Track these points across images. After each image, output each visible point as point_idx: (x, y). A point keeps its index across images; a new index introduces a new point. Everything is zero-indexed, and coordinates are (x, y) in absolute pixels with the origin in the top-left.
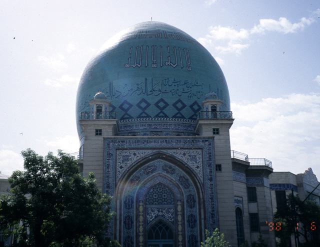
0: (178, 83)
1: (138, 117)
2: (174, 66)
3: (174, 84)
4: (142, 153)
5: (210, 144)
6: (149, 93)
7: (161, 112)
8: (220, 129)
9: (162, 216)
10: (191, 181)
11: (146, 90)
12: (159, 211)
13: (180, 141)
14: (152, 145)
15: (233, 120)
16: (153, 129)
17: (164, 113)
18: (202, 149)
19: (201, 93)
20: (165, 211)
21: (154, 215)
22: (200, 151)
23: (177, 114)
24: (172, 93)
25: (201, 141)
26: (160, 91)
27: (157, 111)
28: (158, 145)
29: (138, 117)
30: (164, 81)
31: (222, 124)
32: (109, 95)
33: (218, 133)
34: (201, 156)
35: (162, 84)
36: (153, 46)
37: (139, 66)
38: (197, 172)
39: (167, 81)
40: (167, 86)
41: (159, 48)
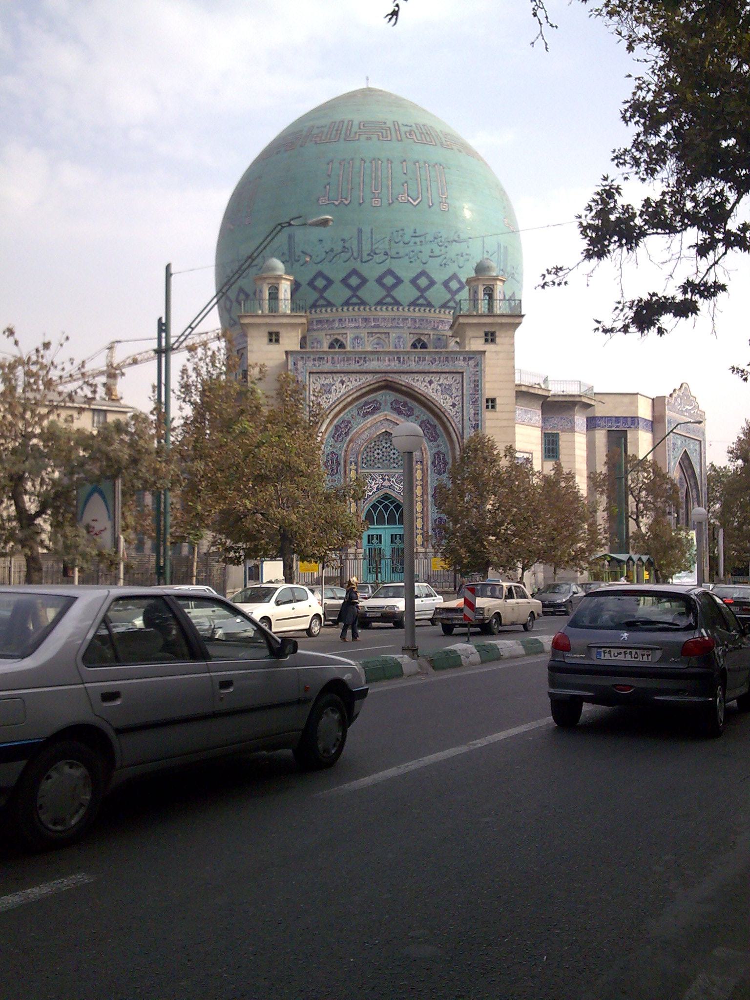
0: (422, 239)
1: (343, 305)
2: (415, 203)
3: (414, 240)
4: (356, 380)
5: (476, 365)
6: (365, 258)
8: (497, 334)
9: (389, 487)
10: (440, 428)
11: (360, 250)
12: (384, 480)
13: (424, 359)
14: (373, 365)
15: (523, 316)
16: (373, 327)
17: (393, 298)
18: (462, 373)
19: (466, 257)
20: (394, 479)
21: (376, 486)
22: (458, 377)
23: (418, 299)
24: (410, 258)
25: (462, 358)
26: (386, 254)
27: (380, 293)
28: (383, 366)
29: (343, 305)
30: (395, 234)
31: (501, 324)
32: (288, 258)
33: (493, 341)
34: (459, 386)
35: (390, 240)
36: (374, 159)
37: (347, 202)
38: (452, 414)
39: (401, 233)
40: (401, 244)
41: (385, 164)
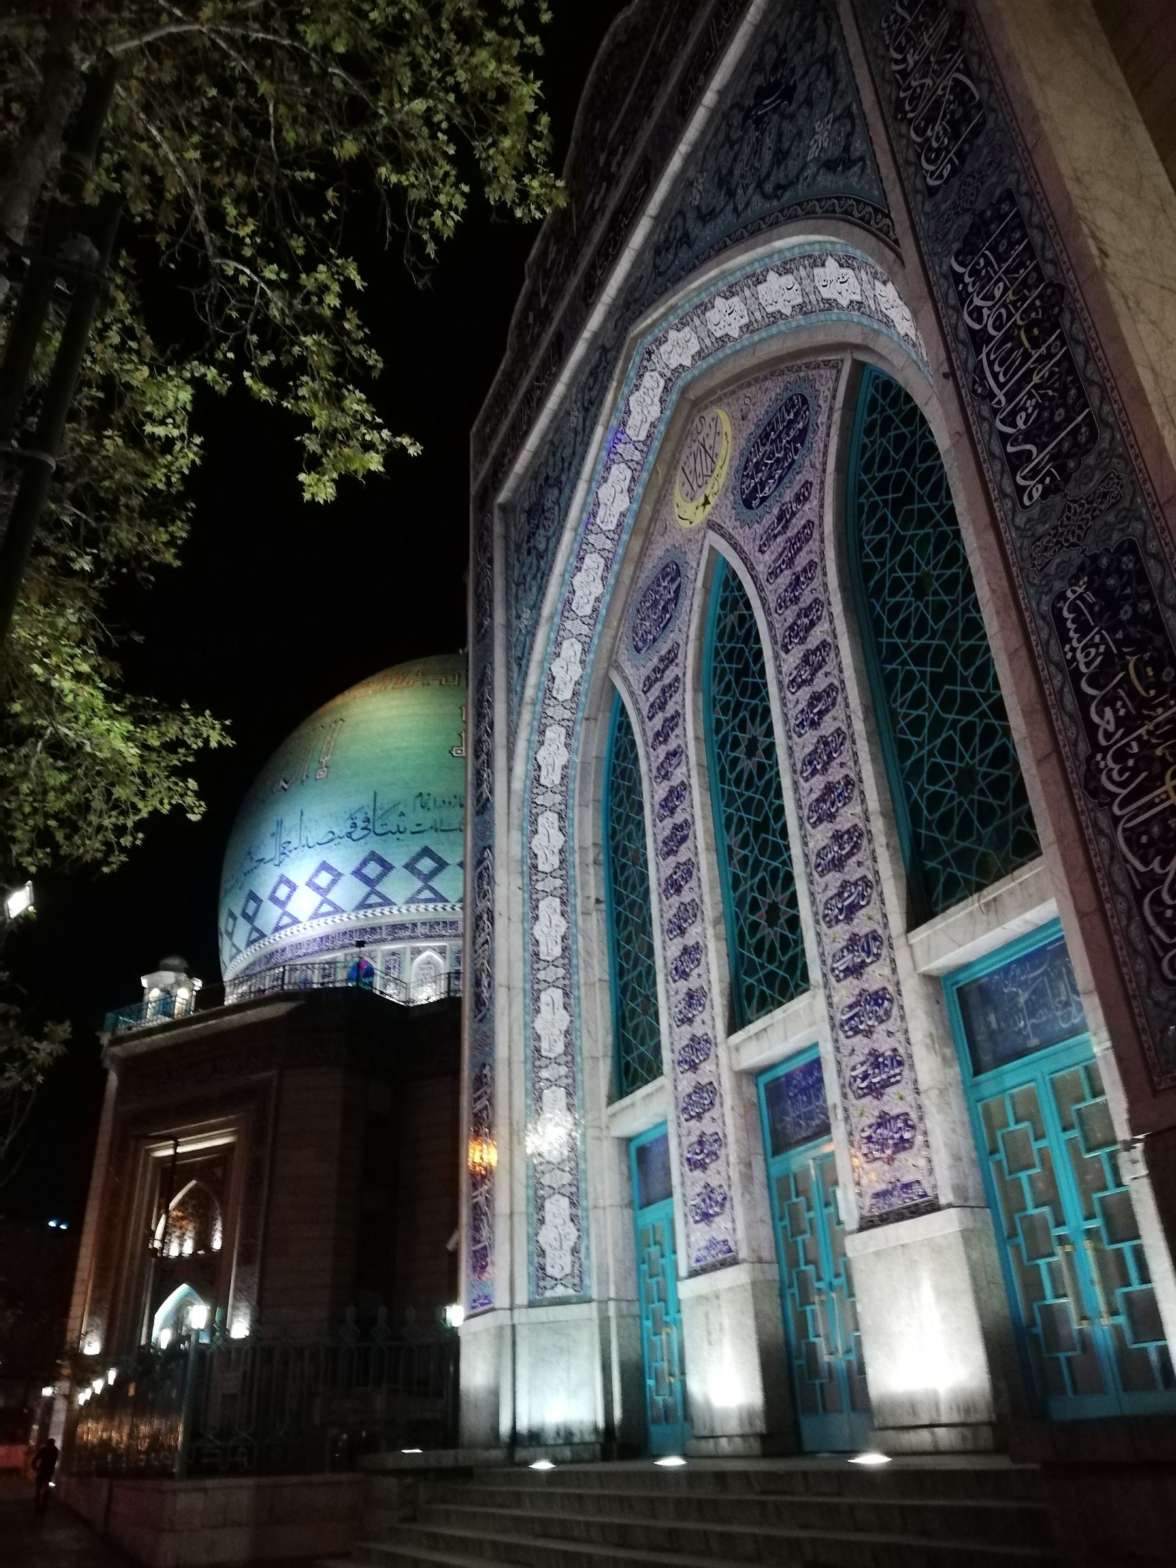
7: (326, 901)
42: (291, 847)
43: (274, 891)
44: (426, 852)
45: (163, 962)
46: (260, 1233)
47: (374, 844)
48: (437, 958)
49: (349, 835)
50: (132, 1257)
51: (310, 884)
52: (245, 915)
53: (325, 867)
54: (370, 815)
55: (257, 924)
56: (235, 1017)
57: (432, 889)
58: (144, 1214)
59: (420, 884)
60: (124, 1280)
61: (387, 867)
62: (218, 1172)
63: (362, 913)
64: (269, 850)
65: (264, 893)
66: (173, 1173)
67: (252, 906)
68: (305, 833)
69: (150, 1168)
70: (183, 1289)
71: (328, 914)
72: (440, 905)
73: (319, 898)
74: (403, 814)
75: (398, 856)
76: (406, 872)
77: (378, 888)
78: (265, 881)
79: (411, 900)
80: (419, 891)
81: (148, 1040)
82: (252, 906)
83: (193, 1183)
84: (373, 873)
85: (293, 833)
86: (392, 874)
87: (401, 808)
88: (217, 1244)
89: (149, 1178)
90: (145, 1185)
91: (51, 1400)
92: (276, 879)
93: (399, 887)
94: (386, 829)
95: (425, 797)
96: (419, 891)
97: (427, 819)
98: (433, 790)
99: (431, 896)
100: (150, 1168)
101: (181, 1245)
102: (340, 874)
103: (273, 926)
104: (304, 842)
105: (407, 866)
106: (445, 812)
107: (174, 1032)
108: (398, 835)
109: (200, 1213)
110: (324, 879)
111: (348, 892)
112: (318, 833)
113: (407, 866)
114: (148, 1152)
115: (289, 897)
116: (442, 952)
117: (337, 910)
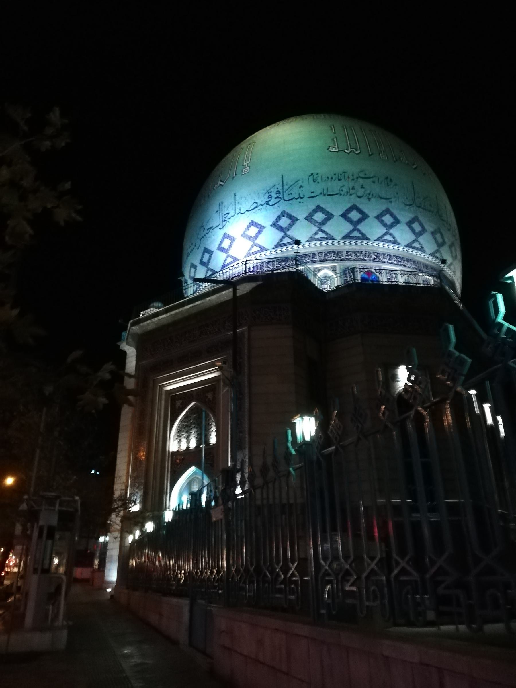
42: (230, 216)
43: (221, 242)
44: (318, 209)
45: (152, 305)
46: (247, 429)
47: (284, 206)
48: (331, 273)
49: (267, 203)
50: (156, 451)
51: (244, 235)
52: (202, 263)
53: (253, 224)
54: (280, 189)
55: (211, 266)
56: (214, 297)
57: (324, 232)
58: (162, 425)
59: (316, 229)
60: (152, 464)
61: (294, 220)
62: (210, 396)
63: (279, 249)
64: (215, 221)
65: (213, 246)
66: (177, 400)
67: (207, 256)
68: (238, 206)
69: (163, 397)
70: (192, 469)
71: (257, 252)
72: (330, 241)
73: (250, 243)
74: (301, 187)
75: (300, 212)
76: (306, 222)
77: (289, 233)
78: (215, 239)
79: (310, 240)
80: (316, 233)
81: (156, 319)
82: (207, 256)
83: (193, 403)
84: (284, 224)
85: (230, 208)
86: (297, 224)
87: (300, 183)
88: (213, 440)
89: (163, 403)
90: (161, 407)
91: (105, 544)
92: (221, 237)
93: (302, 231)
94: (291, 197)
95: (315, 176)
96: (316, 233)
97: (318, 188)
98: (319, 171)
99: (324, 236)
100: (163, 397)
101: (188, 442)
102: (263, 227)
103: (221, 265)
104: (238, 211)
105: (306, 218)
106: (329, 184)
107: (173, 312)
108: (299, 200)
109: (196, 423)
110: (253, 231)
111: (269, 238)
112: (247, 204)
113: (306, 218)
114: (161, 387)
115: (230, 246)
116: (334, 269)
117: (263, 249)
